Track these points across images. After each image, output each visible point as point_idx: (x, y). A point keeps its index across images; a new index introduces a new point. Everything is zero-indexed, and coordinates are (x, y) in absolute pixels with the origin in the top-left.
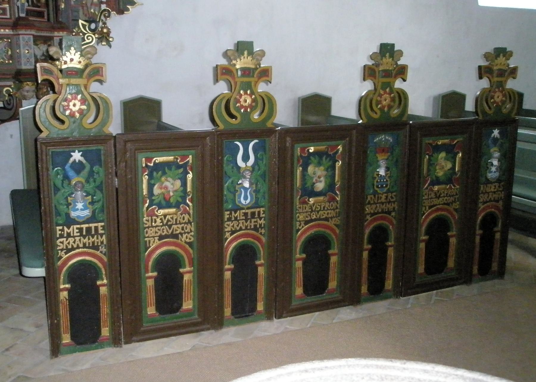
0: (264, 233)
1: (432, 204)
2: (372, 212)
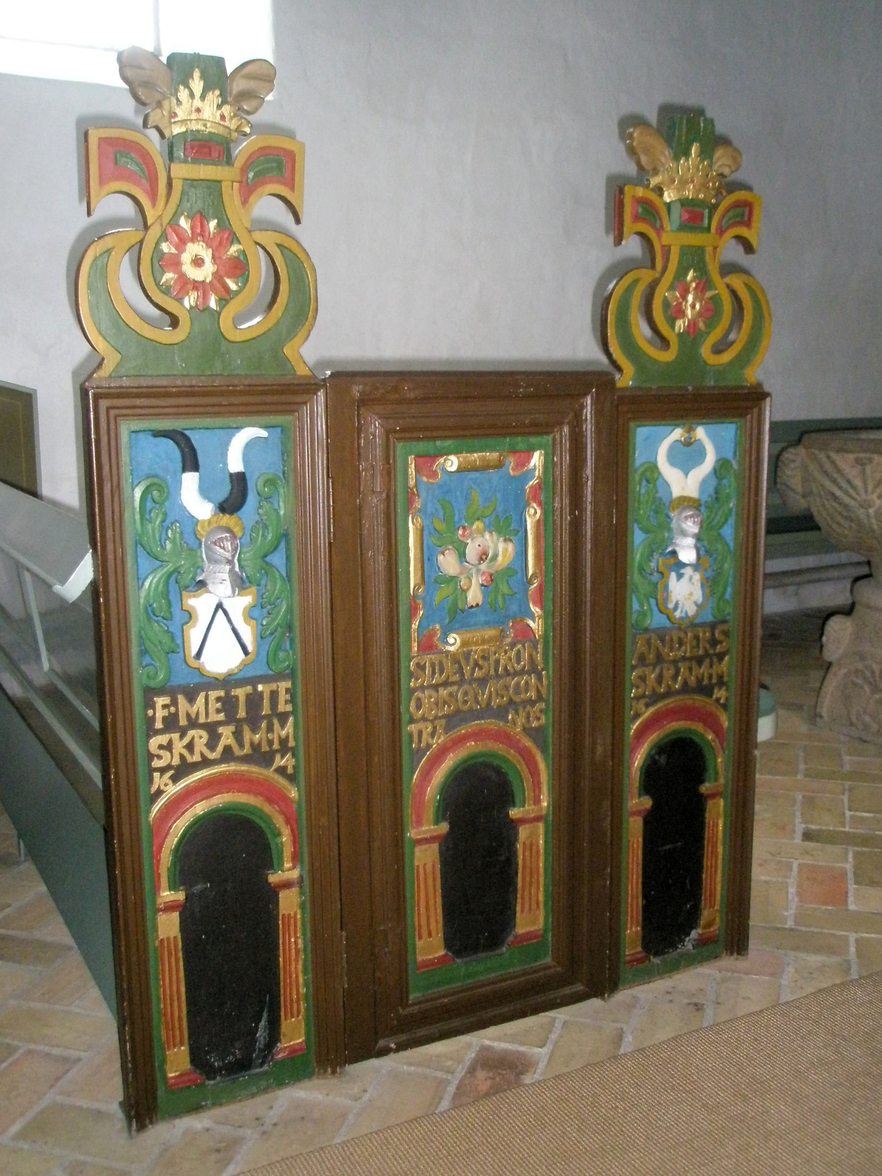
0: (294, 767)
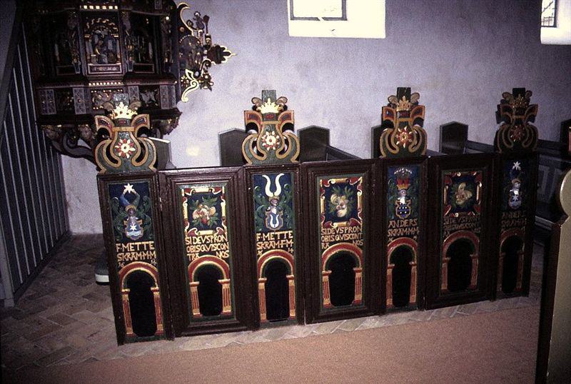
1: (453, 229)
2: (395, 235)
